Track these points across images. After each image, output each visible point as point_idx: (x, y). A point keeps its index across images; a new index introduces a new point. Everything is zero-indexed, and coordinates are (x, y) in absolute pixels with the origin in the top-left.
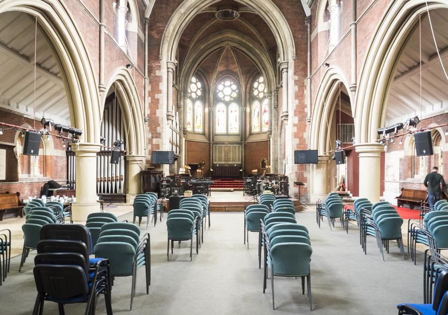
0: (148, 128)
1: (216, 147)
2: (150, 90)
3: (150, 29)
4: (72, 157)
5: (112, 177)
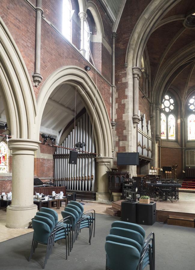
0: (116, 132)
1: (188, 152)
2: (117, 97)
3: (117, 42)
4: (57, 159)
5: (82, 177)
